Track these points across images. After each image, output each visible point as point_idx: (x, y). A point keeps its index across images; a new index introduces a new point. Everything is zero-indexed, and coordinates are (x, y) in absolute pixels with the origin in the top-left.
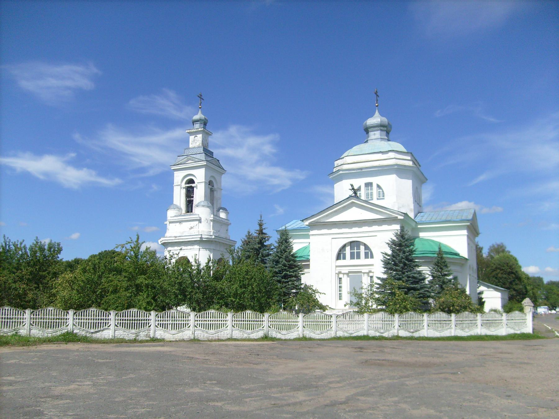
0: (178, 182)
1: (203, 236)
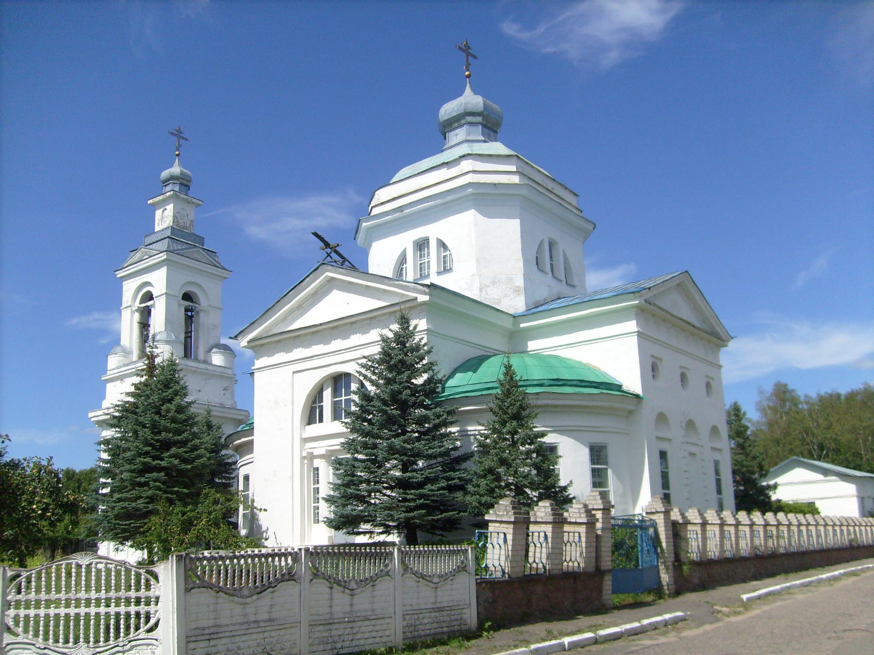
0: (128, 301)
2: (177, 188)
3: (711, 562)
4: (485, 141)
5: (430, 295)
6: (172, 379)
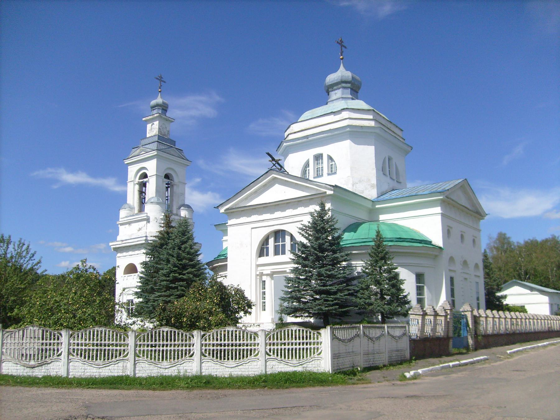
0: (131, 178)
1: (149, 238)
2: (160, 112)
3: (488, 336)
4: (353, 99)
5: (334, 191)
6: (186, 230)
